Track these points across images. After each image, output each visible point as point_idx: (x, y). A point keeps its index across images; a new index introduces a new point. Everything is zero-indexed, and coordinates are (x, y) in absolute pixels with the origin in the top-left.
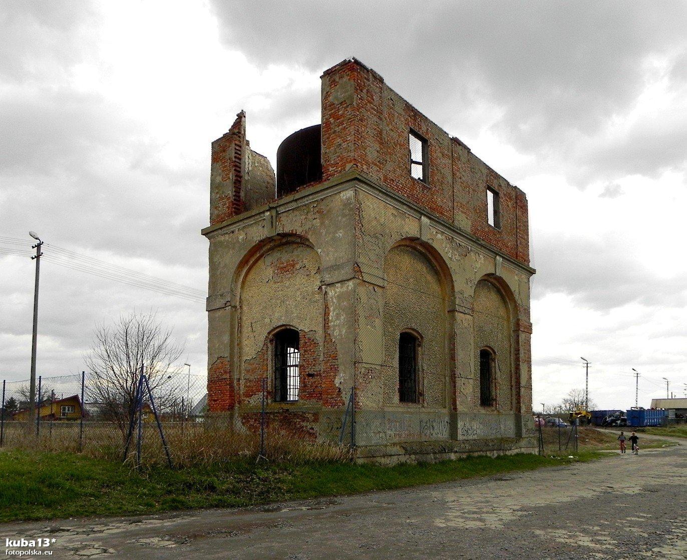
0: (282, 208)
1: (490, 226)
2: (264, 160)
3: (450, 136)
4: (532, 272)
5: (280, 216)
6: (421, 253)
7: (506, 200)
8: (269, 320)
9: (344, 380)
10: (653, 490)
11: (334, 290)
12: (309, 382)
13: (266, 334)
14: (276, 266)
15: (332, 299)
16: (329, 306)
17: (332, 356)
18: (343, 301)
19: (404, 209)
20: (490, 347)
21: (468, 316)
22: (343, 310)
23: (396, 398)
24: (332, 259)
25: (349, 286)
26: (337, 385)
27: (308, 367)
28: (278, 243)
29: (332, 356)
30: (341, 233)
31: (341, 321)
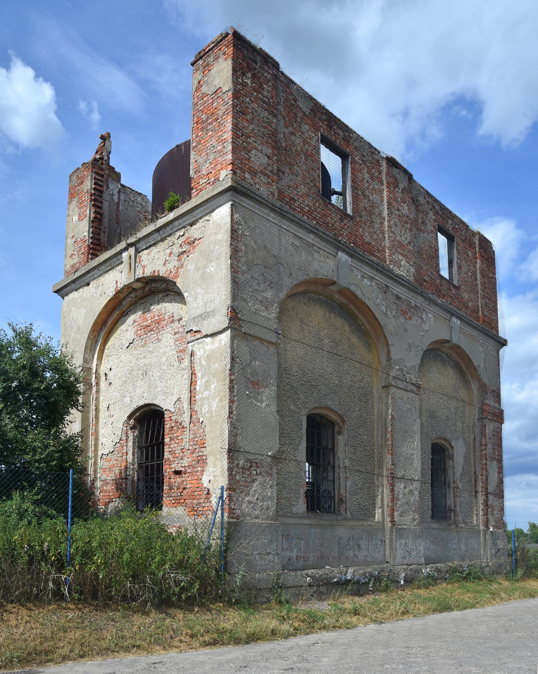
0: (142, 243)
1: (442, 278)
2: (143, 199)
3: (382, 155)
4: (503, 343)
5: (140, 254)
6: (341, 306)
7: (465, 247)
8: (129, 399)
9: (215, 476)
10: (230, 257)
11: (203, 348)
12: (175, 482)
13: (126, 418)
14: (139, 324)
15: (201, 362)
16: (196, 372)
17: (199, 442)
18: (213, 363)
19: (311, 238)
20: (445, 440)
21: (411, 395)
22: (214, 376)
23: (301, 506)
24: (201, 304)
25: (222, 339)
26: (205, 486)
27: (174, 461)
28: (140, 293)
29: (199, 442)
30: (213, 267)
31: (210, 391)
